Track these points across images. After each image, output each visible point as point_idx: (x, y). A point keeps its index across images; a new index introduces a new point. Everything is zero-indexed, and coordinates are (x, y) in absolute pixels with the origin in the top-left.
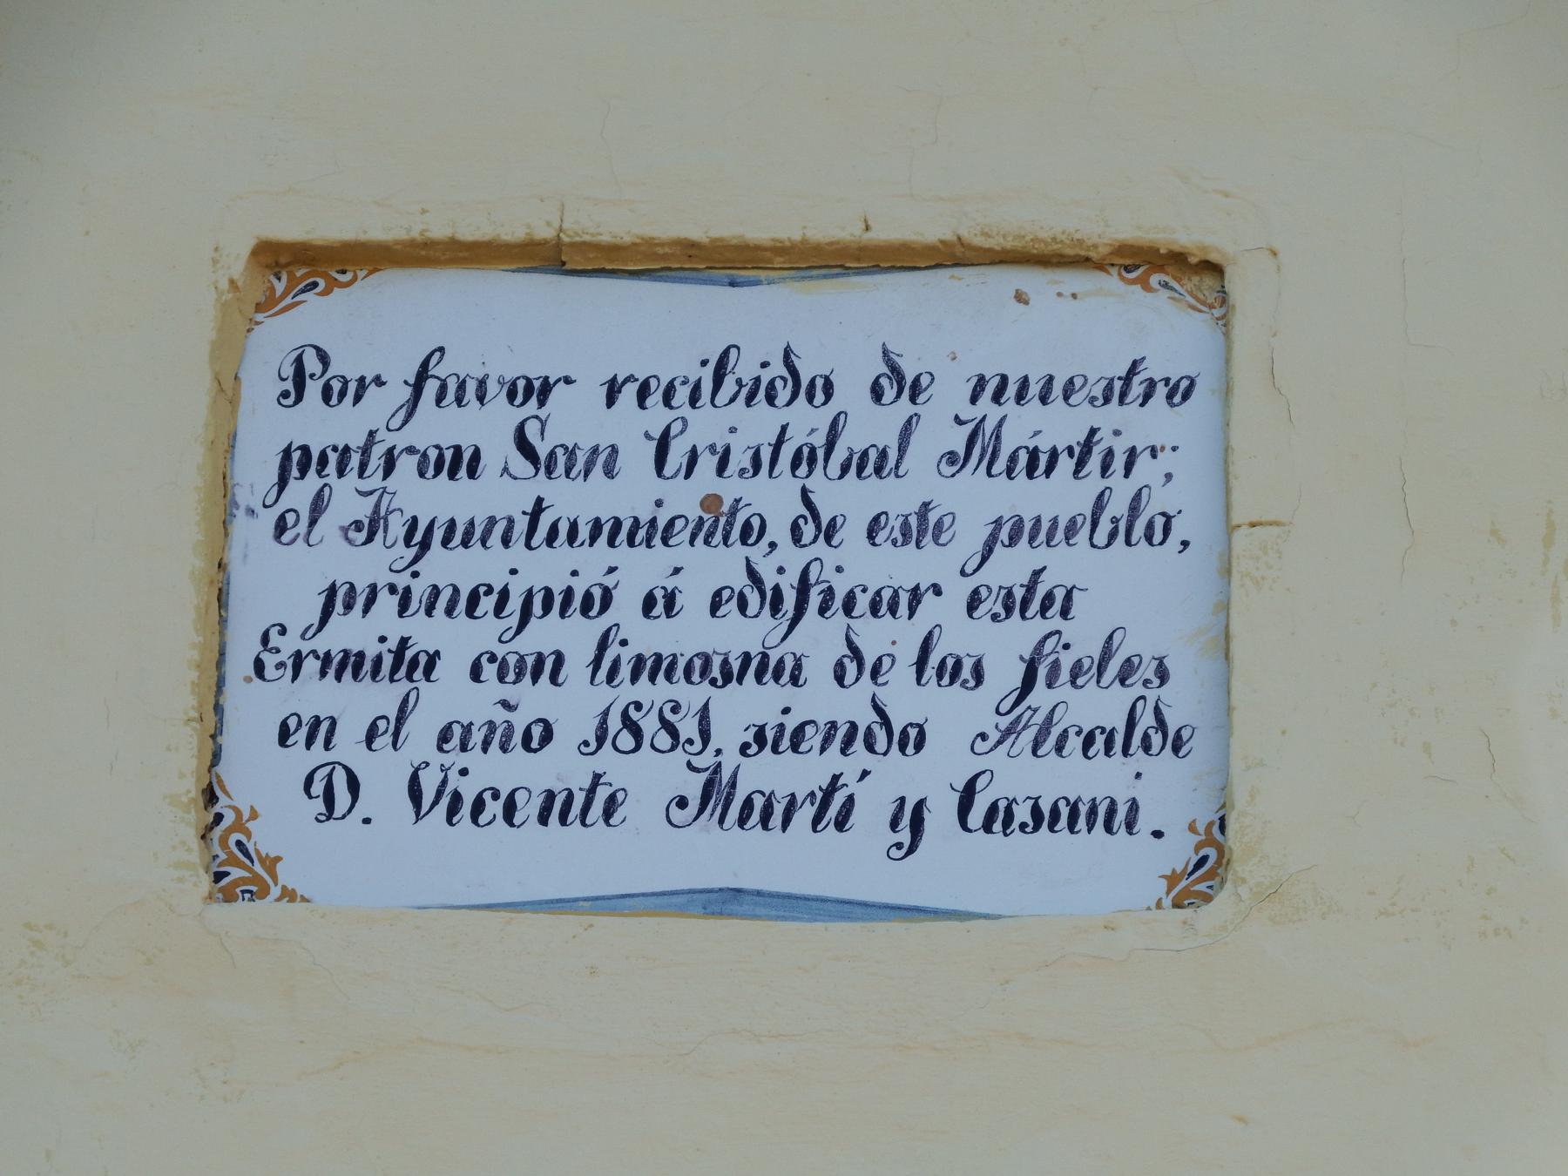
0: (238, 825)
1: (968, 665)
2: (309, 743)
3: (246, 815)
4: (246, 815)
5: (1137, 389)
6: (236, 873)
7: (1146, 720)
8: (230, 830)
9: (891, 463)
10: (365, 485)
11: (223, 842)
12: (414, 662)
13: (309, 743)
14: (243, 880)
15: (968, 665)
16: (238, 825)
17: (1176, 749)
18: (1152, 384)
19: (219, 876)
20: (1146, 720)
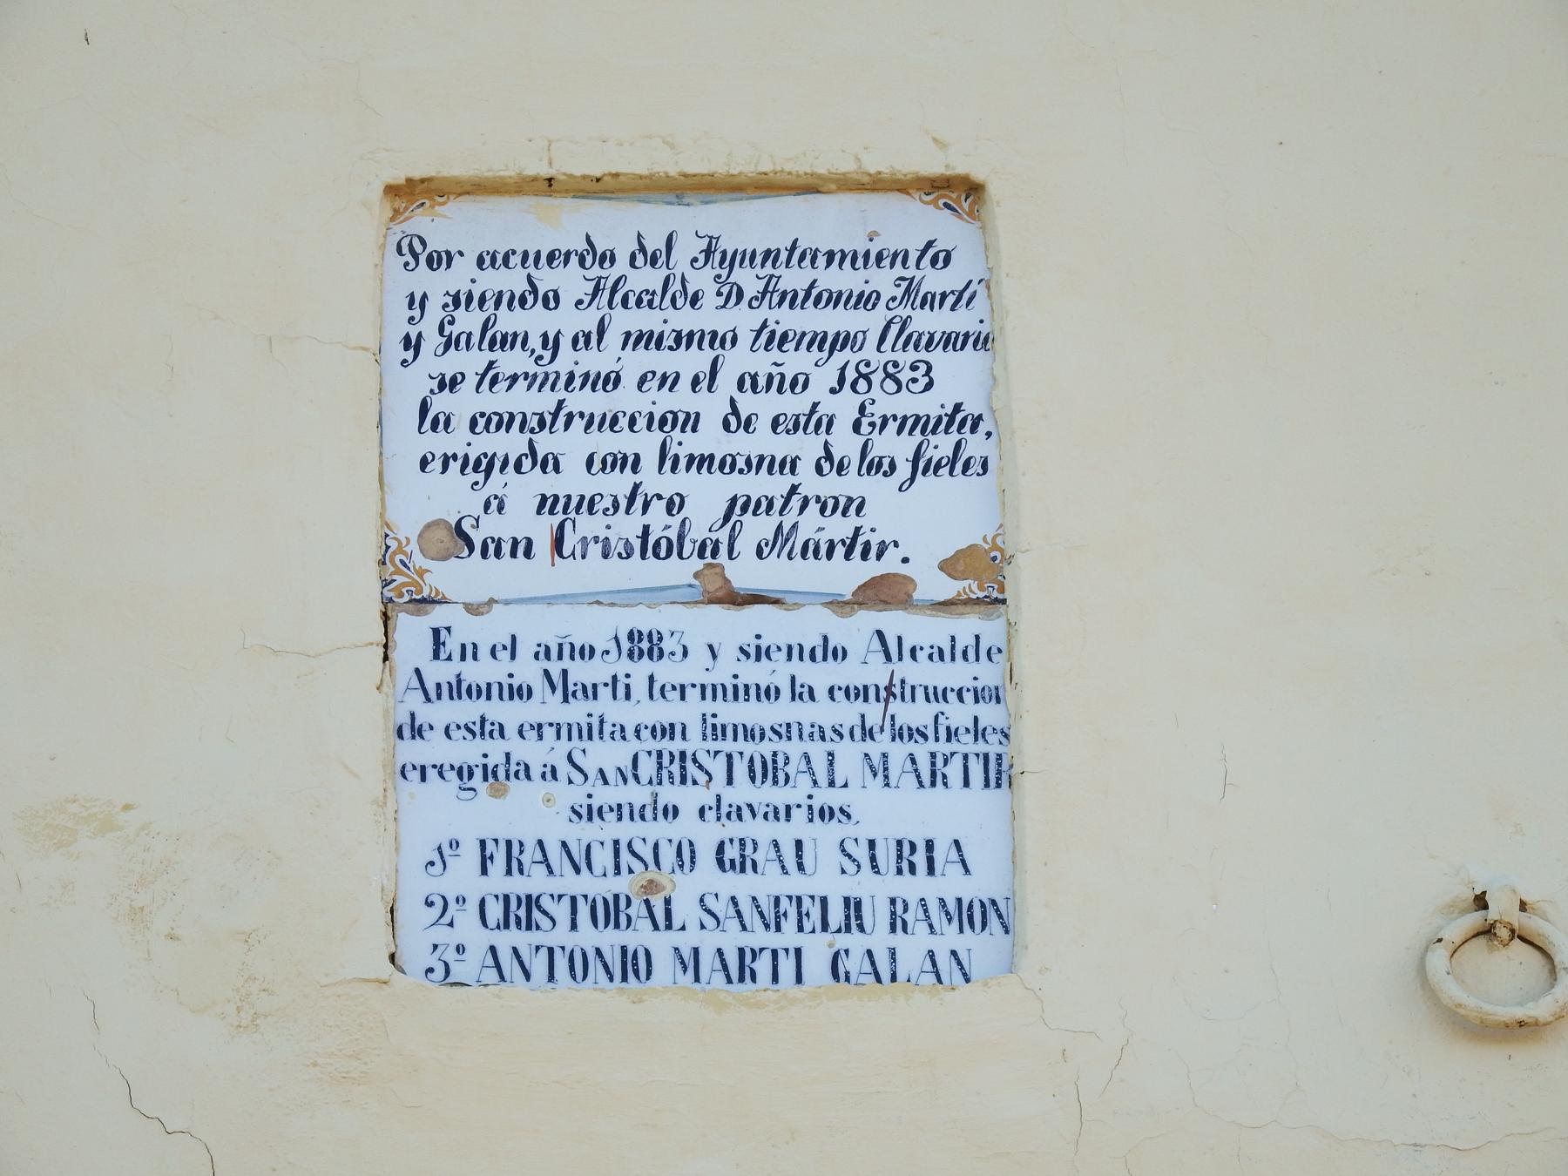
0: (400, 550)
1: (886, 462)
2: (892, 265)
3: (404, 542)
4: (404, 542)
5: (561, 420)
6: (400, 579)
7: (676, 286)
8: (395, 553)
9: (799, 301)
10: (762, 273)
11: (392, 561)
12: (819, 422)
13: (892, 265)
14: (404, 584)
15: (886, 462)
16: (400, 550)
17: (693, 304)
18: (570, 417)
19: (386, 583)
20: (676, 286)
